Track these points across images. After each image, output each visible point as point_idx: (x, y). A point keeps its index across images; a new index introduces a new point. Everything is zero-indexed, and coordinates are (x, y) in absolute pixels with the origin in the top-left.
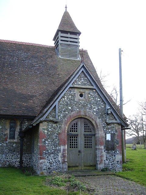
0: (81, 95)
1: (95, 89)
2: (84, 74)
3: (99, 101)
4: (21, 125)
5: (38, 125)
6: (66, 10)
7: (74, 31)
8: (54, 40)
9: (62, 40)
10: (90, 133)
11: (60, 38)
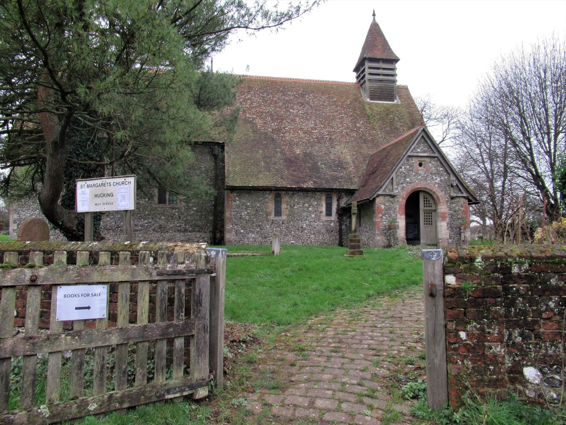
0: (420, 165)
1: (437, 157)
2: (425, 140)
3: (442, 171)
4: (338, 200)
5: (374, 199)
6: (374, 19)
7: (389, 58)
8: (356, 70)
9: (370, 74)
10: (430, 208)
11: (367, 71)
